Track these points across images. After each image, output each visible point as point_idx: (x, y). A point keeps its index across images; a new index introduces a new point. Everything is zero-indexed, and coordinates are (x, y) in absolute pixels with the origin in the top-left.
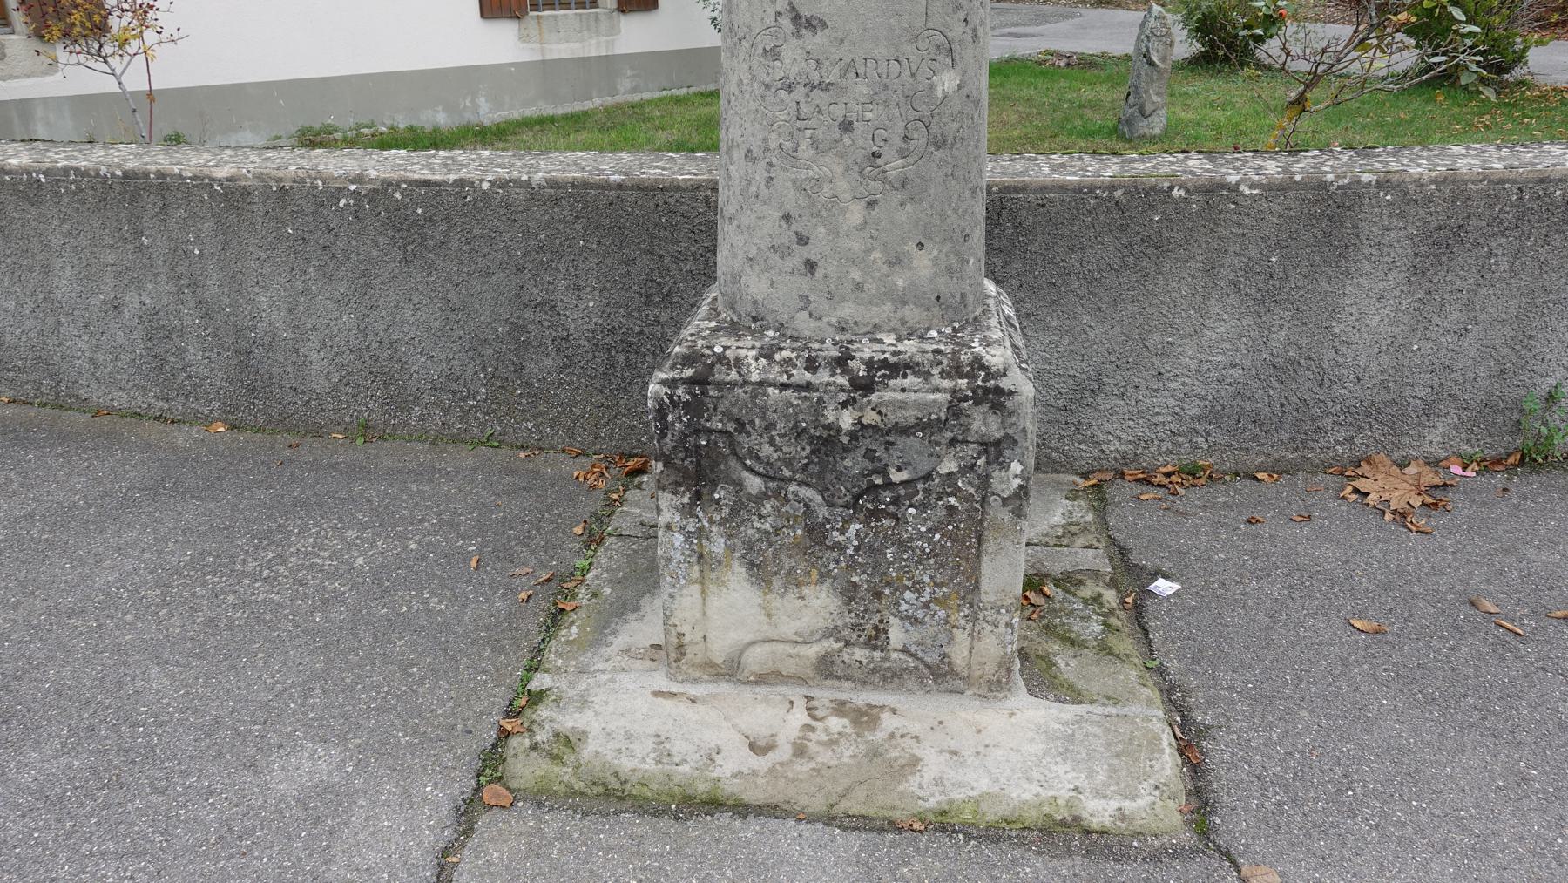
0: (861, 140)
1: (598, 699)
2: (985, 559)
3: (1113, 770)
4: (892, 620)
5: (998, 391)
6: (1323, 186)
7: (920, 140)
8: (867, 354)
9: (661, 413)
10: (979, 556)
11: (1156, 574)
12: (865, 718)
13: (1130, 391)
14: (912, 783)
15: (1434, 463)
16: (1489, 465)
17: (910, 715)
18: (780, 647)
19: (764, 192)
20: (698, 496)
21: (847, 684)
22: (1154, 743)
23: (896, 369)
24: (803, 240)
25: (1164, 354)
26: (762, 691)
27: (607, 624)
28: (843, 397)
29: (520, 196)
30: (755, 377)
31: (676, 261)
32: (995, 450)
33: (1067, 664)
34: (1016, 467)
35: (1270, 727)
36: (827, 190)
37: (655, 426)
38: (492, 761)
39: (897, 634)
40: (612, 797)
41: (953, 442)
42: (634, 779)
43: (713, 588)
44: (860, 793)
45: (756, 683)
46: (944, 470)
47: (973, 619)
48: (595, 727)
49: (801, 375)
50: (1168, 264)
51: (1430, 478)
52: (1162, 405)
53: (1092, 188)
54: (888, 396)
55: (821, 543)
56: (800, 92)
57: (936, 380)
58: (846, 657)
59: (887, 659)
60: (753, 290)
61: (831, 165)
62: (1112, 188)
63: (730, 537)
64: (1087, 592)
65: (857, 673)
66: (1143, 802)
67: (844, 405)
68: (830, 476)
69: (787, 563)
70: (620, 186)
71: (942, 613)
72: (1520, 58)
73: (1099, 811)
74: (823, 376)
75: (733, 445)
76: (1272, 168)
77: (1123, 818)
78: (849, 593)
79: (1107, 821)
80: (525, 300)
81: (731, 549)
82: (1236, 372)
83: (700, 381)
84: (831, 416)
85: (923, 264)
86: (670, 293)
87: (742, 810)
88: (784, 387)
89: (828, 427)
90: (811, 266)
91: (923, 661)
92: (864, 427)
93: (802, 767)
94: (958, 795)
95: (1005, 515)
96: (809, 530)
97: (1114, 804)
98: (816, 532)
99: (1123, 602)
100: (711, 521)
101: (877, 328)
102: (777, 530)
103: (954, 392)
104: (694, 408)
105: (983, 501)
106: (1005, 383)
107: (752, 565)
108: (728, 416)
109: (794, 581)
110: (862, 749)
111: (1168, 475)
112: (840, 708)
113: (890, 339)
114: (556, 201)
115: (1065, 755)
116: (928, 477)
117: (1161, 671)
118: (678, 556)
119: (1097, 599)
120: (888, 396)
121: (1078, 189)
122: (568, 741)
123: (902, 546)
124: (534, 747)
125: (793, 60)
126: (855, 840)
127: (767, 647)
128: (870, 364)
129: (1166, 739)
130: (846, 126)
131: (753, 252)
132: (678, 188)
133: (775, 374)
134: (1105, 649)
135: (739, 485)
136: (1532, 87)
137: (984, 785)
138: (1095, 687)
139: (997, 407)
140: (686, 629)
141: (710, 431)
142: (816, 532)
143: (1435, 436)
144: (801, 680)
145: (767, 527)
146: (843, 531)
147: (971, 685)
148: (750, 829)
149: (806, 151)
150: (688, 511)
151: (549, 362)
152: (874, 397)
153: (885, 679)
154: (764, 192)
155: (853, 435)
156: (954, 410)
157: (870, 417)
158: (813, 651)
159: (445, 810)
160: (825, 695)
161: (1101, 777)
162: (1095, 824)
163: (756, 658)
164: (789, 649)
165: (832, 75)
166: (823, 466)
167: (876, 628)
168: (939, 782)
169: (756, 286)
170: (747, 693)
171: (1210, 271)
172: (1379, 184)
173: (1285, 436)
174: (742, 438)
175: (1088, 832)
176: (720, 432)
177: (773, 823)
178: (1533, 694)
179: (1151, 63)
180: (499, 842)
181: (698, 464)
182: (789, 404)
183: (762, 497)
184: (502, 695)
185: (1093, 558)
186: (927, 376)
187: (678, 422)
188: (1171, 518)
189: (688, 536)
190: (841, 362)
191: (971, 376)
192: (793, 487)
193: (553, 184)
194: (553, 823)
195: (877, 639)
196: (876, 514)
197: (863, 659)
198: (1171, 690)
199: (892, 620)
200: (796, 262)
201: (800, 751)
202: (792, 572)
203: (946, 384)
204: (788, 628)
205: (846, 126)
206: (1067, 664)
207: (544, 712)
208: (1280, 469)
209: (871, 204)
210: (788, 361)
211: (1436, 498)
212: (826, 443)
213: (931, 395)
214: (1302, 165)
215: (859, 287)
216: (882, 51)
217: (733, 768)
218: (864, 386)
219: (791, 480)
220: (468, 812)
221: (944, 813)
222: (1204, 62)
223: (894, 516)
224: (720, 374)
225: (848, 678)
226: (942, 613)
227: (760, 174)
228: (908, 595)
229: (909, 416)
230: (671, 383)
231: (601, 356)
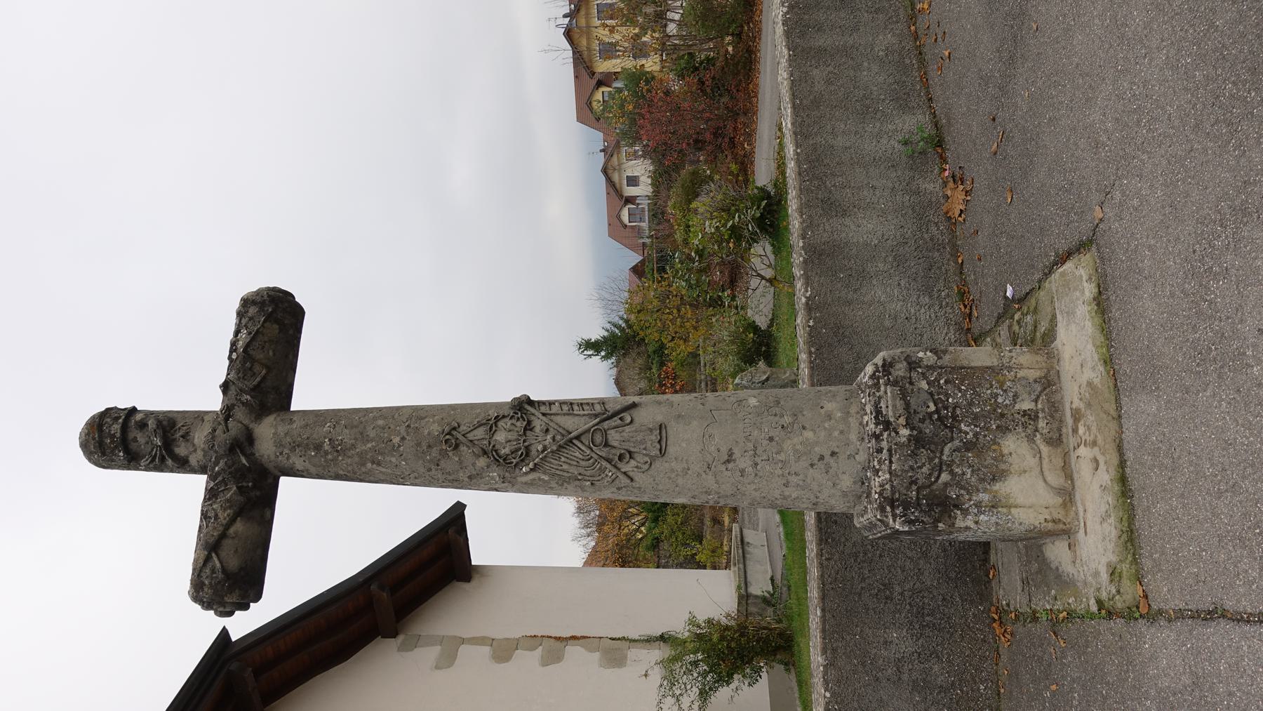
0: (776, 433)
1: (1093, 566)
2: (972, 364)
3: (1075, 289)
4: (1017, 407)
5: (883, 366)
6: (805, 261)
7: (777, 410)
8: (872, 426)
9: (911, 522)
10: (972, 368)
11: (1006, 298)
12: (1077, 416)
13: (918, 331)
14: (1097, 381)
15: (945, 184)
16: (944, 160)
17: (1072, 395)
18: (1045, 466)
19: (801, 477)
20: (956, 506)
21: (1064, 430)
22: (1063, 275)
23: (878, 412)
24: (822, 458)
25: (895, 318)
26: (1076, 476)
27: (1066, 582)
28: (893, 434)
29: (832, 673)
30: (888, 476)
31: (863, 580)
32: (913, 364)
33: (1043, 327)
34: (921, 354)
35: (1051, 226)
36: (798, 447)
37: (918, 526)
38: (1130, 615)
39: (1026, 405)
40: (1130, 538)
41: (911, 383)
42: (1119, 526)
43: (1012, 501)
44: (1106, 406)
45: (1072, 480)
46: (926, 387)
47: (1010, 369)
48: (1104, 560)
49: (885, 453)
50: (847, 322)
51: (951, 184)
52: (924, 315)
53: (811, 362)
54: (890, 413)
55: (975, 444)
56: (758, 460)
57: (882, 393)
58: (1045, 431)
59: (1043, 410)
60: (848, 484)
61: (788, 445)
62: (810, 353)
63: (978, 490)
64: (1016, 328)
65: (1055, 425)
66: (1082, 272)
67: (897, 433)
68: (936, 439)
69: (989, 461)
70: (823, 610)
71: (1008, 384)
72: (762, 189)
73: (1089, 290)
74: (884, 444)
75: (923, 487)
76: (799, 285)
77: (1090, 279)
78: (1003, 430)
79: (1093, 285)
80: (896, 678)
81: (985, 490)
82: (902, 283)
83: (892, 502)
84: (904, 440)
85: (830, 406)
86: (884, 585)
87: (1122, 464)
88: (891, 462)
89: (909, 440)
90: (833, 454)
91: (1041, 392)
92: (907, 424)
93: (1100, 441)
94: (1096, 357)
95: (947, 357)
96: (968, 450)
97: (1085, 284)
98: (969, 446)
99: (1019, 309)
100: (970, 500)
101: (861, 424)
102: (970, 466)
103: (886, 385)
104: (906, 505)
105: (941, 368)
106: (880, 363)
107: (993, 479)
108: (908, 488)
109: (1001, 458)
110: (1088, 412)
111: (965, 307)
112: (1075, 431)
113: (866, 418)
114: (834, 650)
115: (1074, 313)
116: (931, 394)
117: (1040, 281)
118: (994, 518)
119: (1018, 322)
120: (890, 413)
121: (812, 368)
122: (1113, 573)
123: (971, 404)
124: (1118, 592)
125: (744, 462)
126: (1124, 400)
127: (1046, 473)
128: (877, 424)
129: (1061, 270)
130: (771, 439)
131: (830, 483)
132: (822, 576)
133: (885, 467)
134: (1035, 311)
135: (946, 484)
136: (777, 180)
137: (1090, 346)
138: (1049, 309)
139: (891, 365)
140: (1042, 518)
141: (918, 498)
142: (969, 446)
143: (930, 187)
144: (1066, 455)
145: (969, 471)
146: (967, 433)
147: (1052, 368)
148: (1129, 455)
149: (782, 457)
150: (966, 512)
151: (936, 668)
152: (892, 420)
153: (1056, 411)
154: (801, 477)
155: (912, 429)
156: (895, 383)
157: (902, 421)
158: (1045, 449)
159: (1153, 630)
160: (1072, 441)
161: (1078, 293)
162: (1095, 290)
163: (1056, 479)
164: (1045, 461)
165: (750, 445)
166: (930, 443)
167: (1024, 416)
168: (1093, 369)
169: (846, 482)
170: (1078, 483)
171: (849, 303)
172: (804, 238)
173: (937, 254)
174: (920, 482)
175: (1100, 292)
176: (918, 493)
177: (1126, 445)
178: (1022, 122)
179: (767, 379)
180: (1166, 595)
181: (937, 505)
182: (899, 459)
183: (952, 472)
184: (1104, 625)
185: (1003, 331)
186: (880, 398)
187: (914, 514)
188: (984, 299)
189: (981, 513)
190: (877, 437)
191: (878, 378)
192: (945, 458)
193: (824, 651)
194: (1147, 564)
195: (1032, 416)
196: (954, 417)
197: (1047, 420)
198: (1046, 274)
199: (1017, 407)
200: (832, 461)
201: (1094, 443)
202: (995, 459)
203: (882, 388)
204: (1031, 461)
205: (771, 439)
206: (1043, 327)
207: (1104, 596)
208: (955, 254)
209: (804, 428)
210: (879, 462)
211: (958, 179)
212: (918, 441)
213: (889, 396)
214: (797, 272)
215: (842, 432)
216: (741, 426)
217: (1106, 476)
218: (887, 425)
219: (940, 458)
220: (1153, 616)
221: (1105, 362)
222: (770, 359)
223: (954, 409)
224: (888, 494)
225: (1059, 430)
226: (1008, 384)
227: (794, 479)
228: (1000, 400)
229: (900, 404)
230: (894, 516)
231: (927, 630)
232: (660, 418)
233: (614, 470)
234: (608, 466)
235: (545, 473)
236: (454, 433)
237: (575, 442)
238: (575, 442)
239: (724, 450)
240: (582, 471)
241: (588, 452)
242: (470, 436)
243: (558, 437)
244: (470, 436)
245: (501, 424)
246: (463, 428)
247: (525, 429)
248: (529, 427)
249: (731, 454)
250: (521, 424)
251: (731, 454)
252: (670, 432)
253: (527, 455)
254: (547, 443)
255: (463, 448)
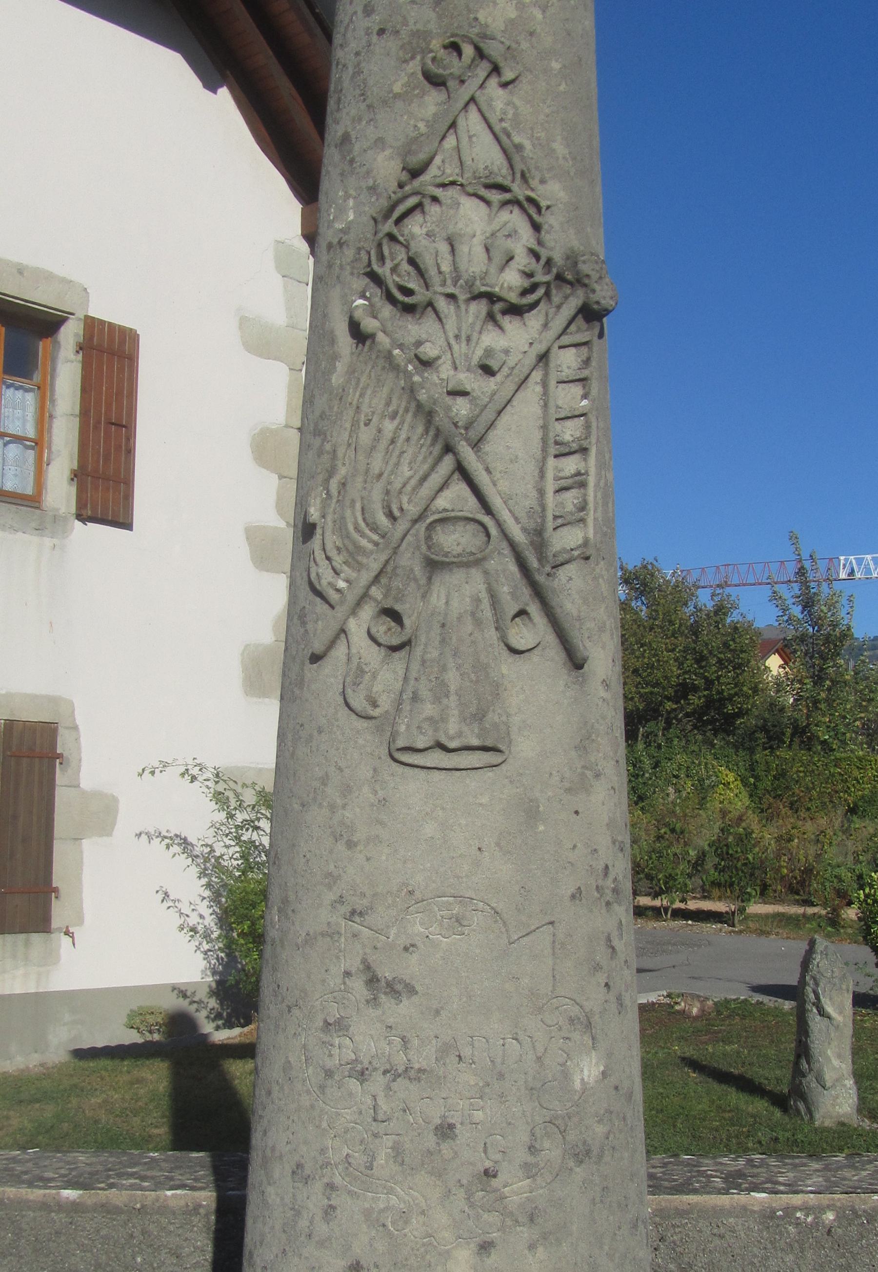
36: (415, 1227)
56: (378, 1082)
130: (446, 1131)
165: (423, 1057)
205: (446, 1131)
209: (485, 1247)
232: (525, 747)
233: (351, 598)
234: (366, 577)
235: (351, 371)
236: (483, 69)
237: (448, 462)
238: (448, 462)
239: (411, 968)
240: (355, 489)
241: (413, 510)
242: (472, 121)
243: (462, 408)
244: (472, 121)
245: (514, 218)
246: (496, 97)
247: (491, 298)
248: (503, 308)
249: (397, 989)
250: (510, 281)
251: (397, 989)
252: (472, 781)
253: (409, 309)
254: (445, 370)
255: (433, 99)
